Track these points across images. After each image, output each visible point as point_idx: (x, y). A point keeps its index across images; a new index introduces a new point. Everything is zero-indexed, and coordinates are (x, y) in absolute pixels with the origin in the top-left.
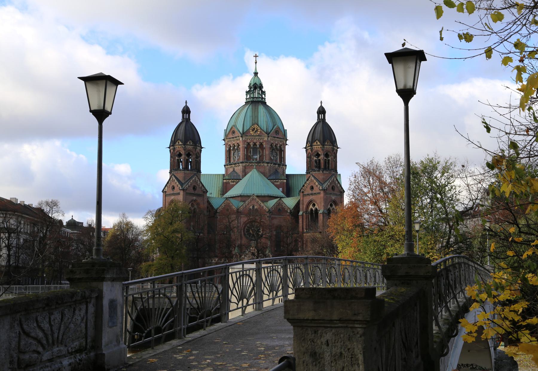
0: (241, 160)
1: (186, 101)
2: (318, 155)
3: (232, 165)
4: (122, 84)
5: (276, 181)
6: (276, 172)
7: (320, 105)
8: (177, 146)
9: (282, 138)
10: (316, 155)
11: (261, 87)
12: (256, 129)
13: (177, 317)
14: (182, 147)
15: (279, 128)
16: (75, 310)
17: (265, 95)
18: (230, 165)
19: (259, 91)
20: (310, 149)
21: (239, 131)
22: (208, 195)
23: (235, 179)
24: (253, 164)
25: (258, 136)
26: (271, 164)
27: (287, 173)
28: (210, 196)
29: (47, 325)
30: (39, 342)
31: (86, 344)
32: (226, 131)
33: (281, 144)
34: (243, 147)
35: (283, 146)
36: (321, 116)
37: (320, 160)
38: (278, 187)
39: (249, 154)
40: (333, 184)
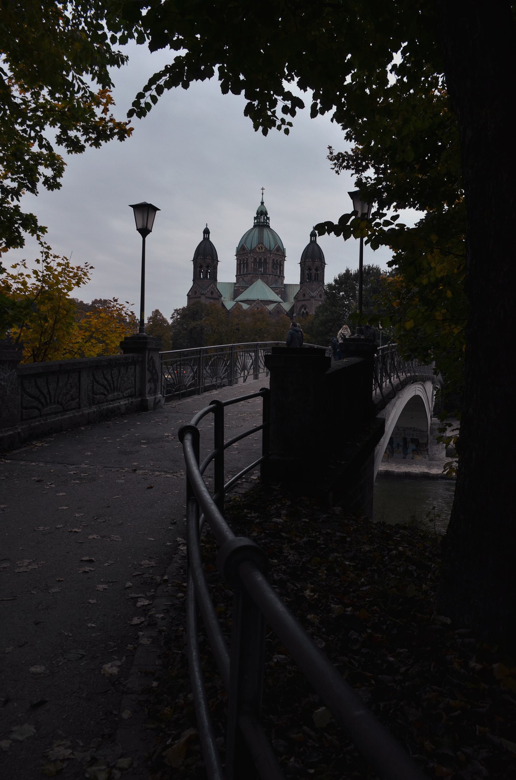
1: (207, 224)
4: (159, 210)
11: (266, 214)
12: (260, 248)
13: (197, 379)
16: (127, 368)
18: (240, 275)
19: (265, 217)
22: (222, 298)
24: (259, 275)
25: (263, 253)
26: (273, 275)
27: (285, 283)
28: (224, 299)
29: (110, 377)
30: (105, 387)
31: (135, 392)
32: (237, 248)
36: (207, 236)
37: (311, 273)
40: (320, 293)
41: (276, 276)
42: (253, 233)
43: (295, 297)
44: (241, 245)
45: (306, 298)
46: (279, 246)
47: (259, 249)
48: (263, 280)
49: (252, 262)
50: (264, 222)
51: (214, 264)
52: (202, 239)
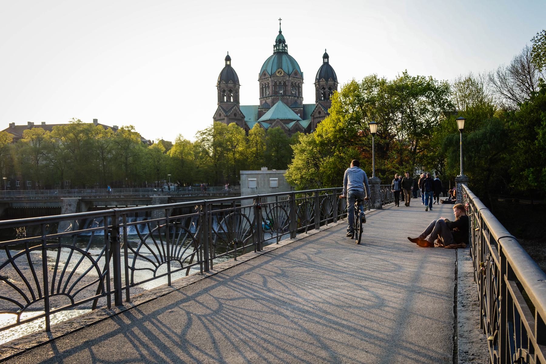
3: (264, 98)
11: (284, 42)
18: (263, 98)
22: (246, 119)
25: (282, 77)
32: (260, 74)
36: (326, 60)
43: (312, 114)
45: (321, 115)
47: (281, 73)
50: (282, 49)
52: (225, 66)
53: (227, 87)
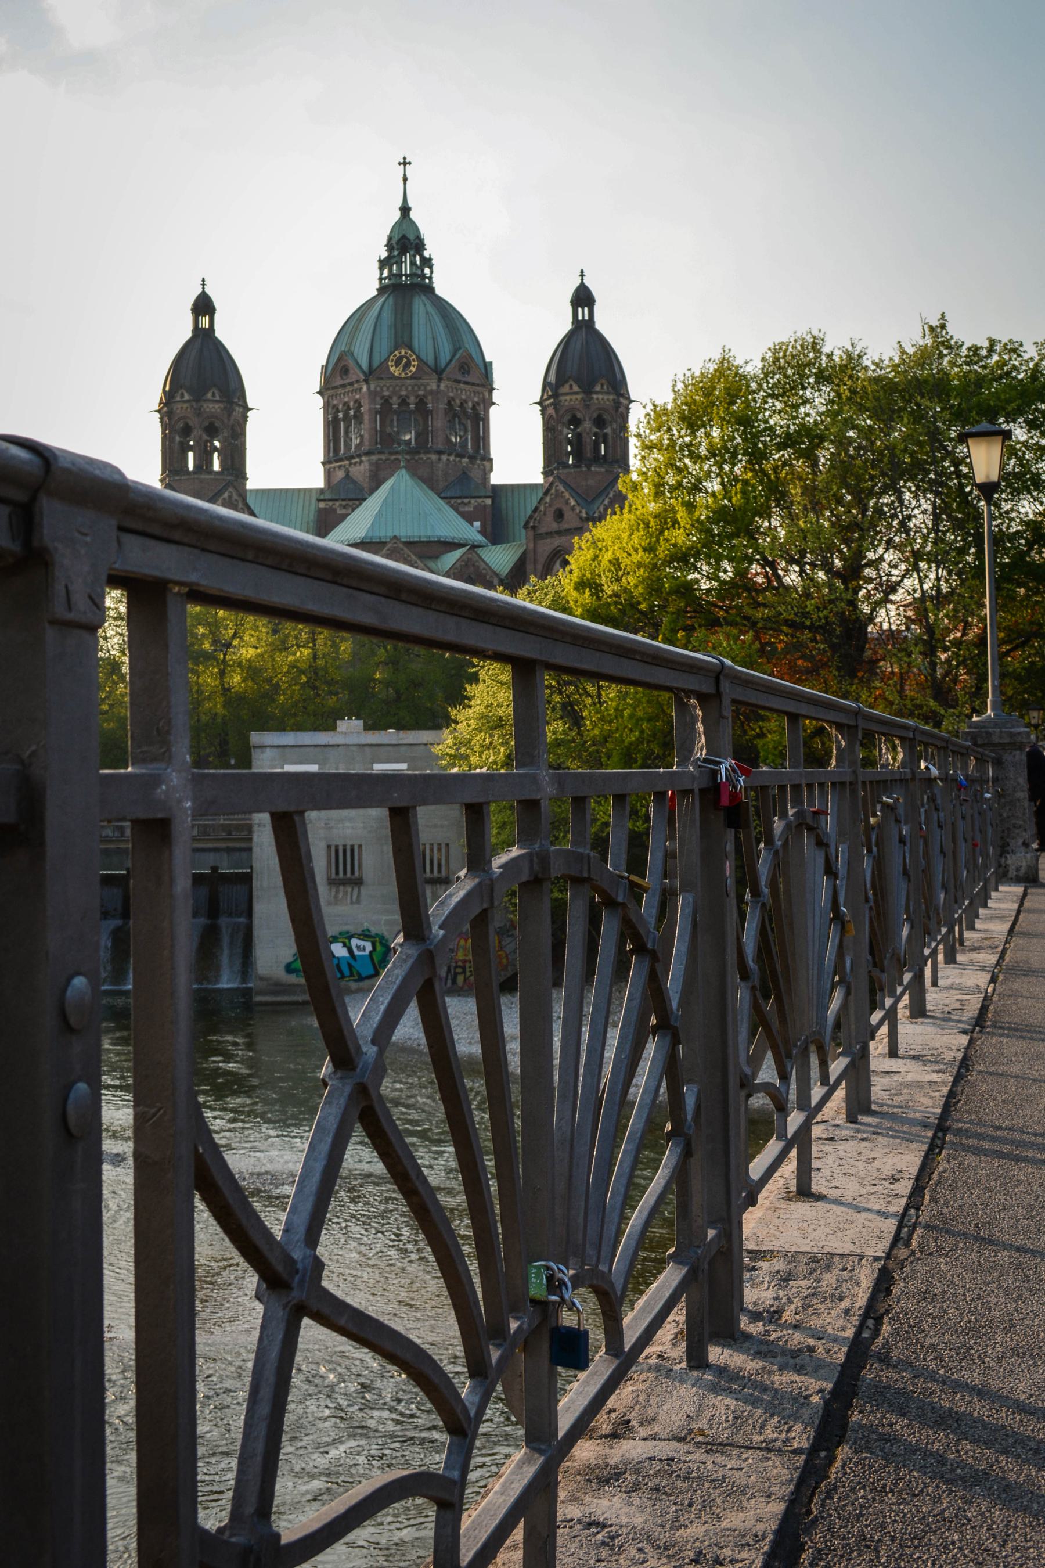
0: (366, 448)
1: (203, 280)
2: (575, 421)
3: (341, 460)
5: (462, 502)
6: (464, 477)
7: (578, 282)
8: (179, 405)
9: (478, 385)
10: (570, 422)
11: (418, 245)
14: (192, 406)
15: (470, 356)
17: (431, 267)
18: (337, 461)
20: (551, 404)
21: (360, 367)
23: (350, 500)
24: (400, 457)
25: (411, 378)
26: (449, 455)
32: (325, 368)
33: (476, 399)
34: (370, 410)
35: (482, 406)
36: (583, 313)
38: (469, 518)
39: (388, 430)
41: (461, 456)
42: (376, 313)
44: (337, 356)
46: (466, 350)
48: (413, 471)
49: (377, 412)
51: (232, 418)
53: (198, 413)
